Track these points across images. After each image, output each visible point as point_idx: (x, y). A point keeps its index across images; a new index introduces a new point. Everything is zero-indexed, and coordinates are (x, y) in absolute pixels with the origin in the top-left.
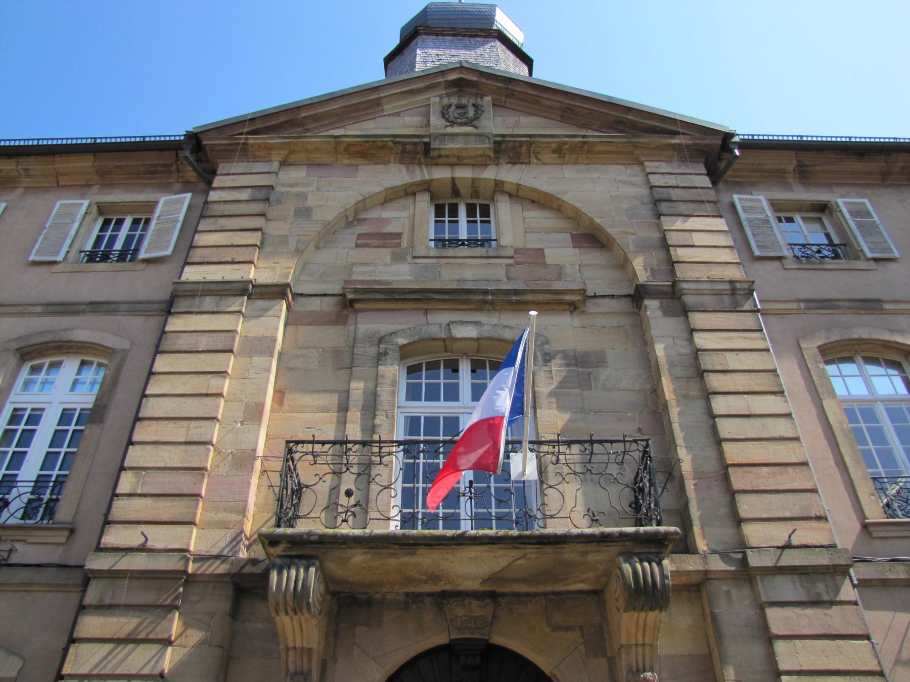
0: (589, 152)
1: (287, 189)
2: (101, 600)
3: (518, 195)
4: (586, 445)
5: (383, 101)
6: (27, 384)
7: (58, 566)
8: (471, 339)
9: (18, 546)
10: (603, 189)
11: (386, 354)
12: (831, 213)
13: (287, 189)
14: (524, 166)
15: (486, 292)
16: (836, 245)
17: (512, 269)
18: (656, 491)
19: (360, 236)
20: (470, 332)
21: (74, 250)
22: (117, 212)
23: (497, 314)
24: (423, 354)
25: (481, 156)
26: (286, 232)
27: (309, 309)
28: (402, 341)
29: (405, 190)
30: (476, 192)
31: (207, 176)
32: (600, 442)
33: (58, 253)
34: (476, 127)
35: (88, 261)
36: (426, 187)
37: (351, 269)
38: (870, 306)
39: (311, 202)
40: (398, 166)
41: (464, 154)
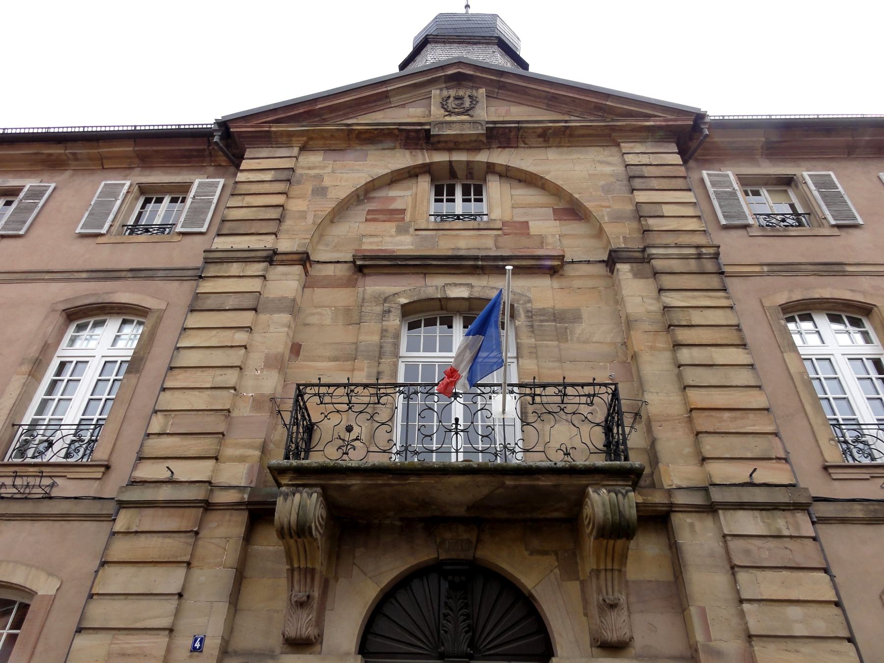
0: (571, 136)
1: (307, 172)
2: (129, 528)
3: (507, 174)
4: (560, 388)
5: (390, 94)
6: (73, 340)
7: (95, 498)
8: (463, 298)
9: (58, 481)
10: (580, 169)
11: (389, 311)
12: (797, 186)
13: (307, 172)
14: (512, 150)
15: (476, 258)
16: (800, 215)
17: (500, 239)
18: (623, 430)
19: (370, 212)
20: (463, 293)
21: (117, 224)
22: (156, 192)
23: (486, 277)
24: (422, 312)
25: (475, 141)
26: (305, 209)
27: (324, 274)
28: (403, 301)
29: (409, 172)
30: (471, 173)
31: (235, 160)
32: (573, 385)
33: (102, 227)
34: (471, 116)
35: (130, 234)
36: (426, 169)
37: (361, 240)
38: (833, 269)
39: (327, 182)
40: (402, 151)
41: (460, 140)
